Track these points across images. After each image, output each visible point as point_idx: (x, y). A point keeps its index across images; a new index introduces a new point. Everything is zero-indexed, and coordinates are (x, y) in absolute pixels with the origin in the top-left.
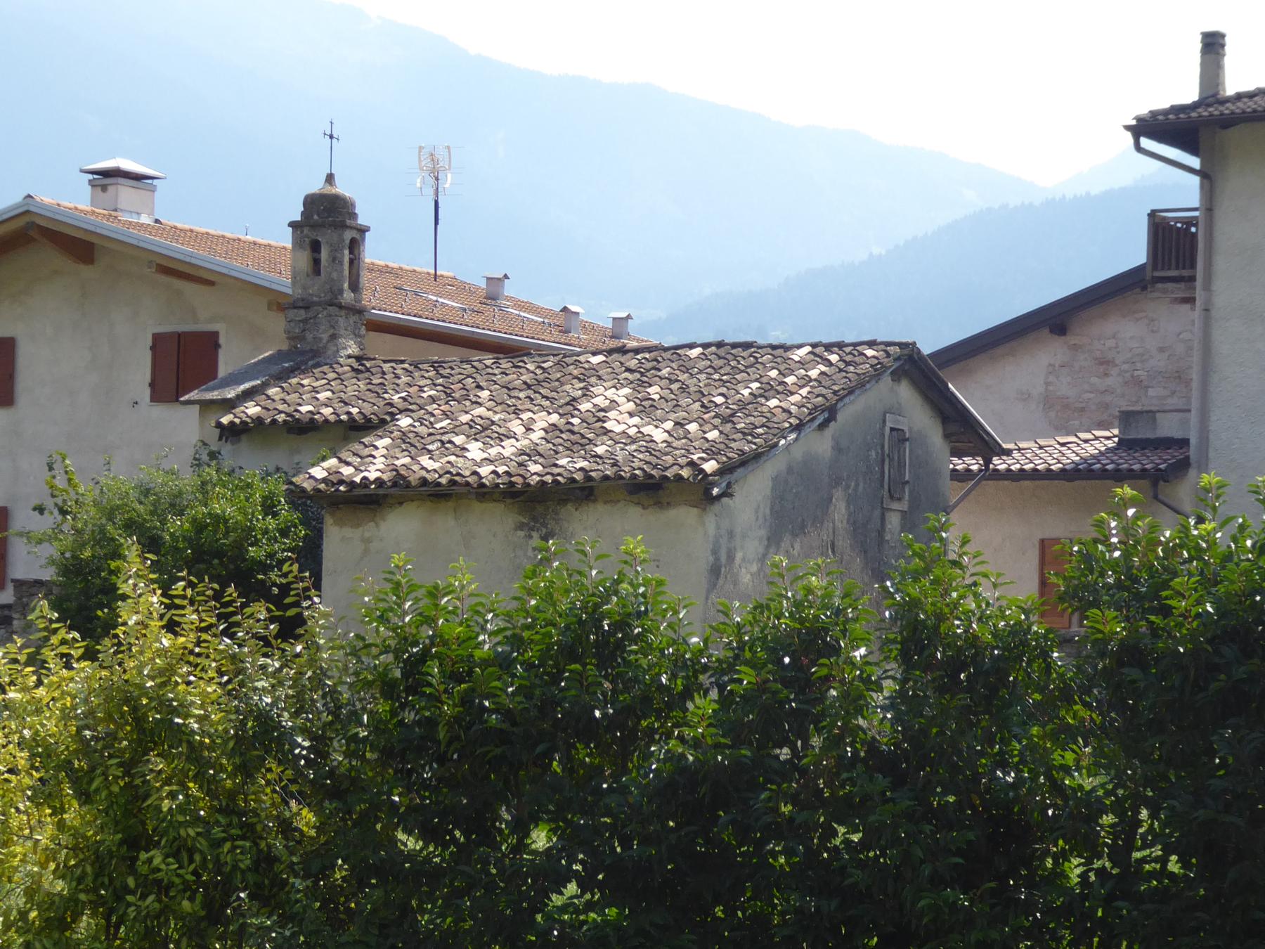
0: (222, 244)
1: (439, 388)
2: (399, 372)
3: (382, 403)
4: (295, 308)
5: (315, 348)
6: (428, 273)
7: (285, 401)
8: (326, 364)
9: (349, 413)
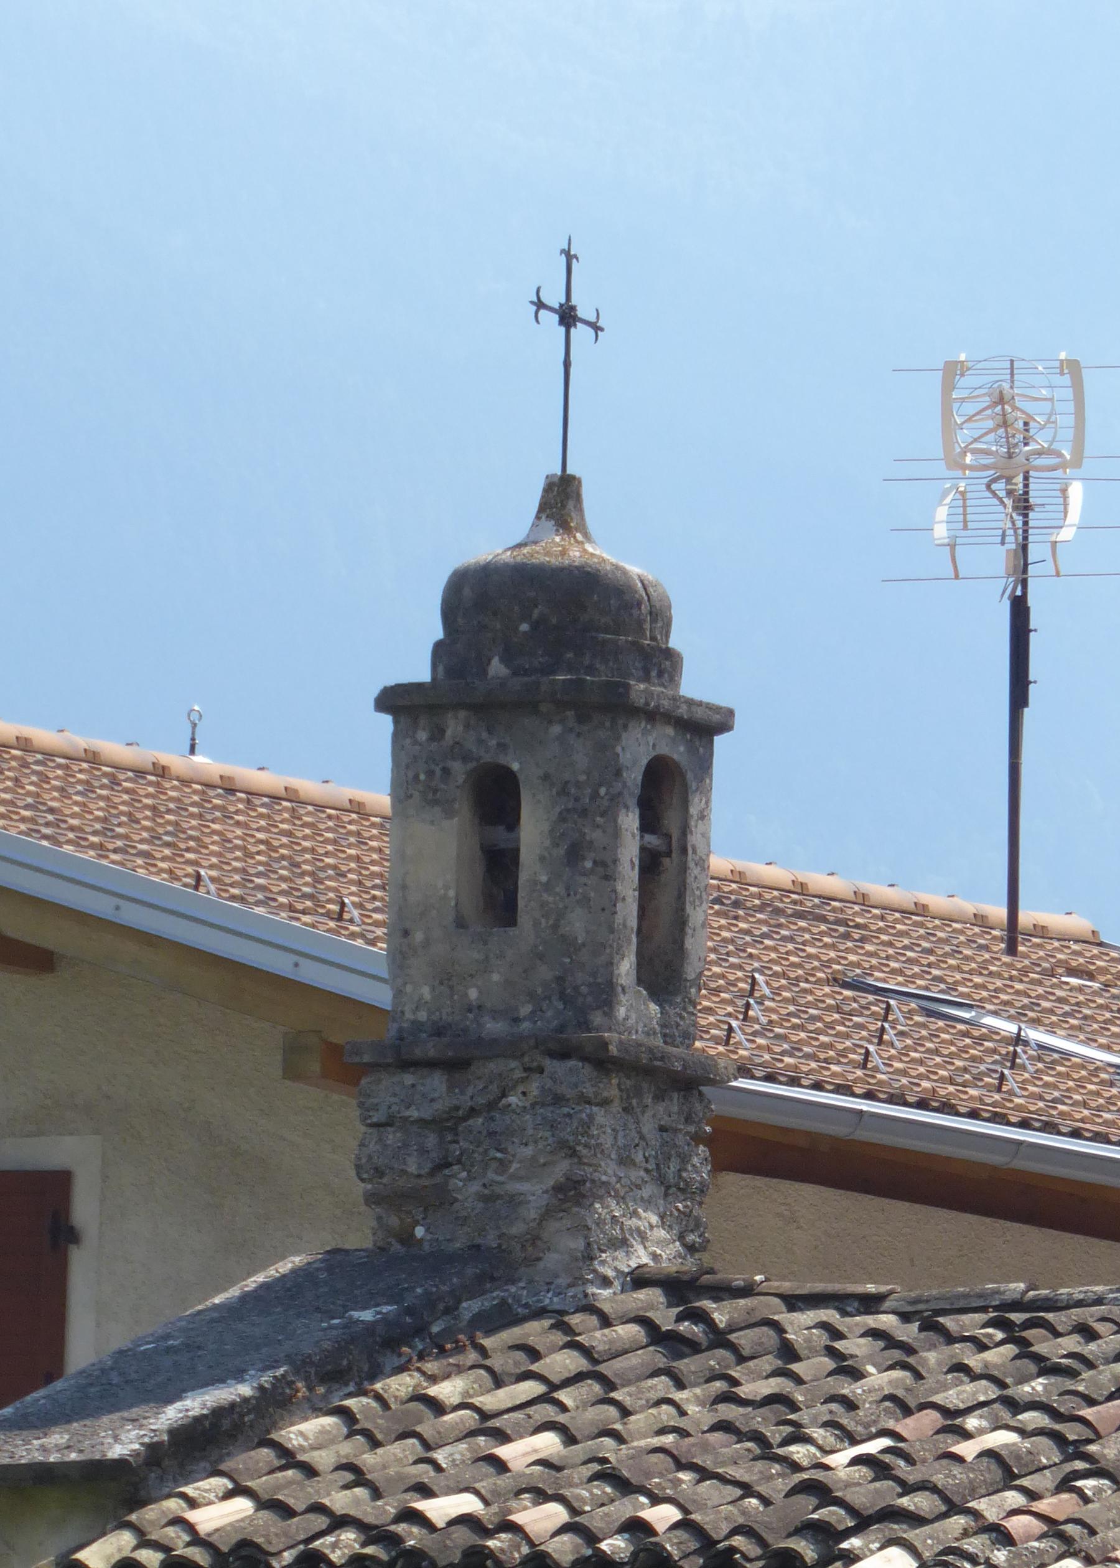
0: (89, 787)
1: (1032, 1418)
2: (855, 1346)
3: (779, 1484)
4: (407, 1065)
5: (491, 1240)
6: (980, 920)
7: (357, 1475)
8: (540, 1313)
9: (636, 1527)
